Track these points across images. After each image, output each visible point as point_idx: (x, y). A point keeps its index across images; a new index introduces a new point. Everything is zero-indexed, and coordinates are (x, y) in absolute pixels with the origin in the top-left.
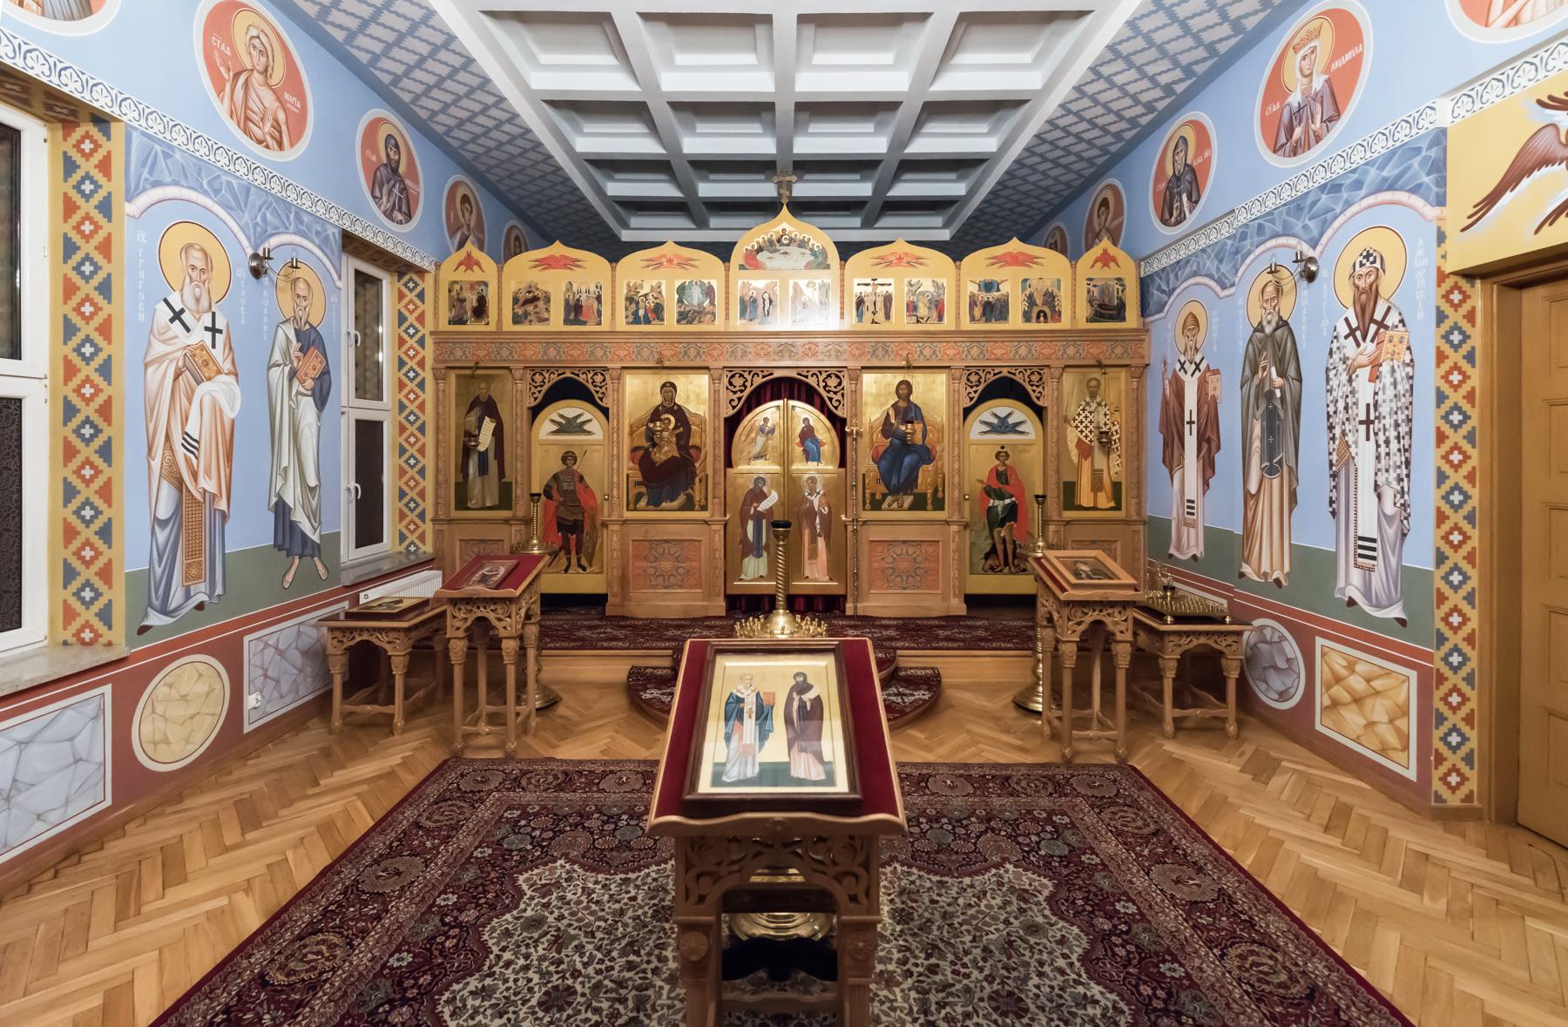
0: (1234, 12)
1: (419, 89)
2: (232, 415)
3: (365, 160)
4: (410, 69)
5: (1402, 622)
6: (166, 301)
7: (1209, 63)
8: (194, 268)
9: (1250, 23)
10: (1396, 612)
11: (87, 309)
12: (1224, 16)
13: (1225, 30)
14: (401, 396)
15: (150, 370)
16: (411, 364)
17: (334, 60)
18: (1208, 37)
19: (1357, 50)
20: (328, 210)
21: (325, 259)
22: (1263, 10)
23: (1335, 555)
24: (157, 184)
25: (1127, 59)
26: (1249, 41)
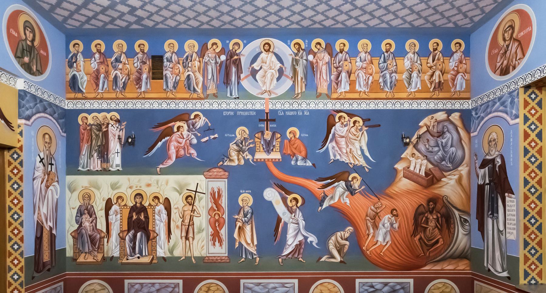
0: (481, 4)
1: (66, 14)
2: (57, 197)
3: (9, 35)
4: (72, 13)
5: (509, 278)
6: (39, 155)
7: (481, 16)
8: (46, 143)
9: (487, 9)
10: (505, 274)
11: (533, 236)
12: (477, 6)
13: (478, 12)
14: (540, 205)
15: (35, 181)
16: (533, 229)
17: (51, 26)
18: (470, 14)
19: (529, 29)
20: (49, 96)
21: (58, 126)
22: (482, 14)
23: (484, 250)
24: (52, 116)
25: (441, 14)
26: (488, 17)
